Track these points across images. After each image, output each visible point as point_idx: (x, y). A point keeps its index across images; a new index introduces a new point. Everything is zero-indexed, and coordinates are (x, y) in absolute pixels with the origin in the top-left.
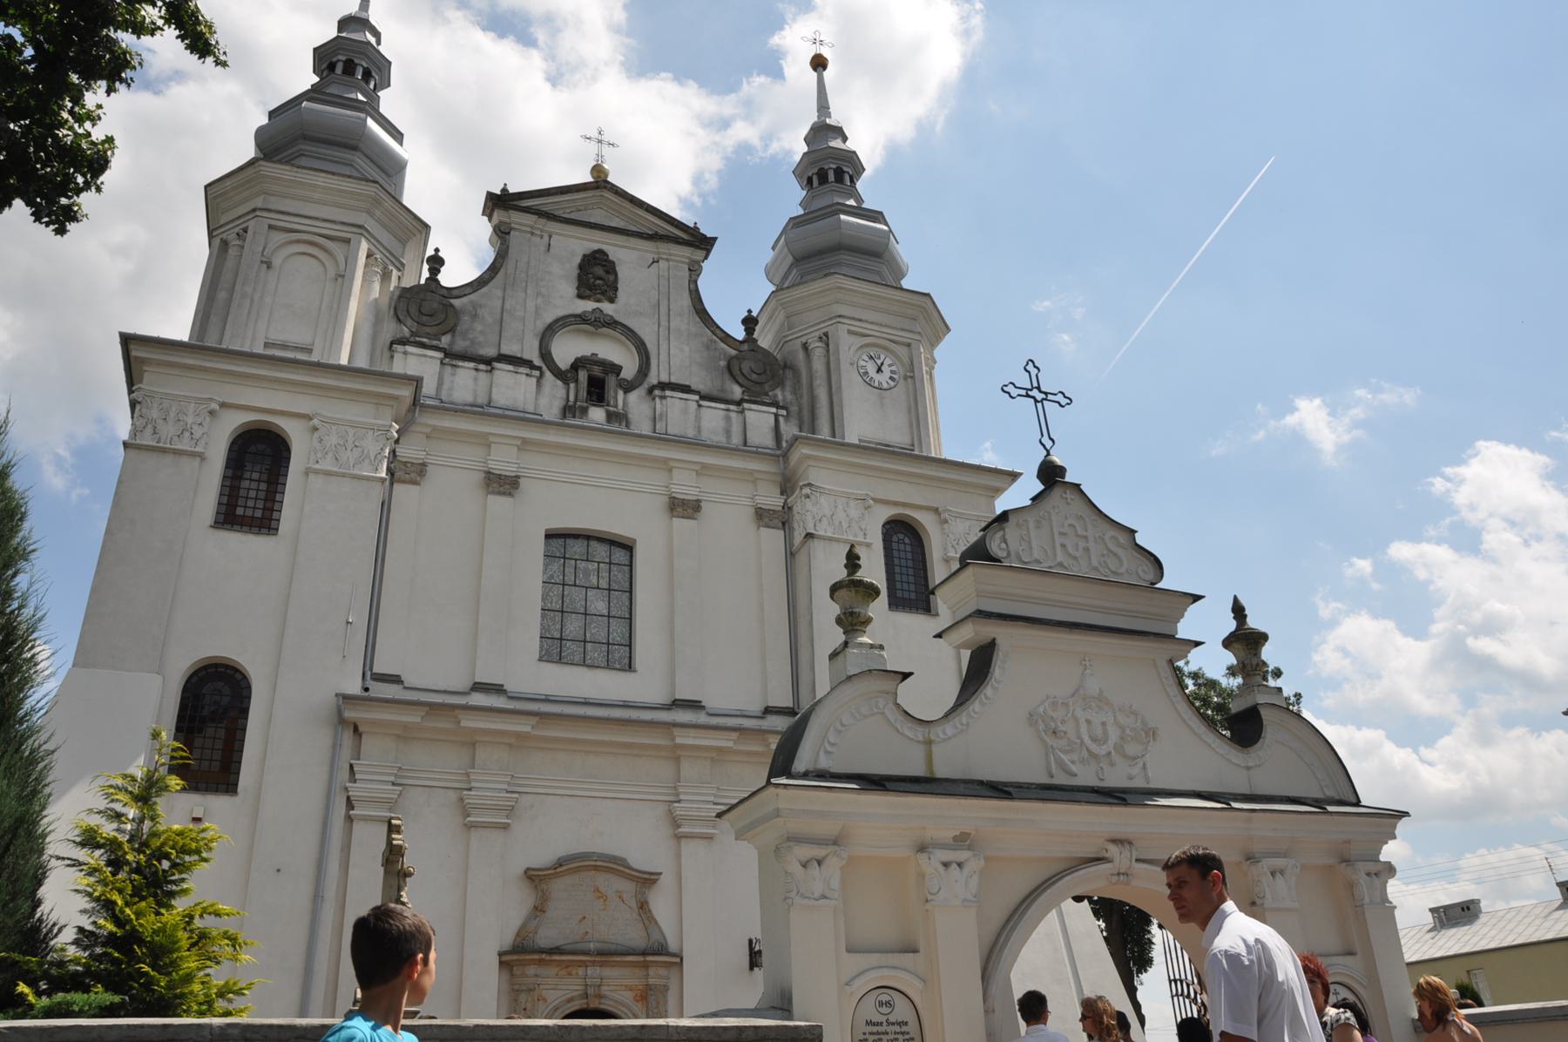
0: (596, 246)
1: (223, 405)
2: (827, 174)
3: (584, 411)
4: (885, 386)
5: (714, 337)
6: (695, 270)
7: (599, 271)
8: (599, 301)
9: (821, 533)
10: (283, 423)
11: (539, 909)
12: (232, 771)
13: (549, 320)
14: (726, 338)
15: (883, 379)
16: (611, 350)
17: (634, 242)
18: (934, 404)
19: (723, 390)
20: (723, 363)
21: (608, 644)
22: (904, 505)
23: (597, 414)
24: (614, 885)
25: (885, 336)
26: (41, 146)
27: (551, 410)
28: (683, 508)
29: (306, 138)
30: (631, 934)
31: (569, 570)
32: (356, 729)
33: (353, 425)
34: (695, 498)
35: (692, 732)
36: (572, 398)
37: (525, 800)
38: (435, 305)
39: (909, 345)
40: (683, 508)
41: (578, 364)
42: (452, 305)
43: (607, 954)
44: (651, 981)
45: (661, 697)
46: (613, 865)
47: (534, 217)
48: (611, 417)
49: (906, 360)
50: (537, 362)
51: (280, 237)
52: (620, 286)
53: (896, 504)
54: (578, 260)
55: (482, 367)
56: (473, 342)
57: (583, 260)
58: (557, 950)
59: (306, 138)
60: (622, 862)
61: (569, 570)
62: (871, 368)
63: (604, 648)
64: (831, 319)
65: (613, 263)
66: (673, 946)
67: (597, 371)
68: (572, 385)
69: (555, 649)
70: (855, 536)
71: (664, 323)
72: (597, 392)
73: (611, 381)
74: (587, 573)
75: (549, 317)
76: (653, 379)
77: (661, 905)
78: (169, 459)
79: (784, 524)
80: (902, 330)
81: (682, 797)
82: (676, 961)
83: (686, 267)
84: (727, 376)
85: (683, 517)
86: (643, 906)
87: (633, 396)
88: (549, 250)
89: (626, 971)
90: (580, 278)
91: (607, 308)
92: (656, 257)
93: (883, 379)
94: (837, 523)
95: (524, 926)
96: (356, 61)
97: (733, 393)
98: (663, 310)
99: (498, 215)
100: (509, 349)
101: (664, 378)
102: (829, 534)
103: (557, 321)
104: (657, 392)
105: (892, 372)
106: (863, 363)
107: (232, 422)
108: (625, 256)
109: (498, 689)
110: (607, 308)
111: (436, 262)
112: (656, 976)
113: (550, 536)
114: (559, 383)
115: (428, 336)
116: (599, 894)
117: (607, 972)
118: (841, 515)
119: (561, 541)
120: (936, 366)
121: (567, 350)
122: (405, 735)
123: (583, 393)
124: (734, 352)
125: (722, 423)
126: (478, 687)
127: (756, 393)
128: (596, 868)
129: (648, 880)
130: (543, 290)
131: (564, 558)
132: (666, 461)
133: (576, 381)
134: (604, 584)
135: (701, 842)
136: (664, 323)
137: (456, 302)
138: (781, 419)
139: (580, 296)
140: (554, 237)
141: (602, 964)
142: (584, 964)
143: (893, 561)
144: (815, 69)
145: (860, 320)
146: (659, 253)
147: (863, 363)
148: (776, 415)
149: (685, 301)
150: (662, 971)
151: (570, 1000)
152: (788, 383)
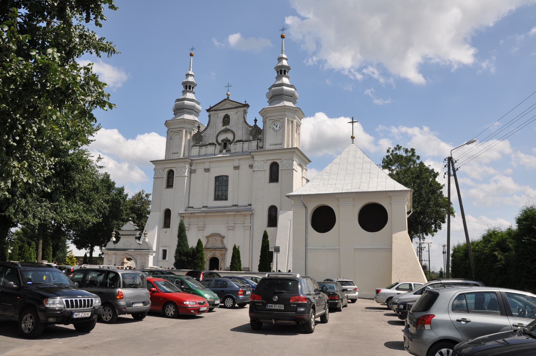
0: (226, 113)
1: (165, 168)
3: (222, 151)
6: (245, 112)
7: (226, 119)
10: (277, 161)
12: (451, 156)
13: (218, 133)
14: (250, 126)
15: (277, 129)
16: (230, 136)
17: (233, 110)
19: (249, 139)
20: (249, 132)
23: (224, 151)
24: (218, 238)
26: (73, 194)
30: (220, 245)
33: (181, 167)
37: (206, 225)
38: (198, 137)
39: (283, 118)
40: (236, 168)
41: (222, 141)
42: (201, 136)
43: (215, 249)
46: (219, 235)
47: (214, 112)
48: (227, 151)
50: (216, 143)
51: (172, 133)
52: (230, 122)
53: (272, 160)
56: (205, 142)
60: (220, 235)
65: (229, 116)
66: (226, 248)
67: (225, 142)
69: (217, 198)
72: (225, 146)
73: (228, 143)
75: (217, 133)
76: (235, 140)
77: (225, 241)
78: (159, 179)
80: (281, 115)
86: (222, 242)
89: (219, 251)
90: (223, 122)
96: (282, 70)
100: (211, 142)
105: (280, 126)
107: (167, 170)
108: (231, 113)
110: (228, 127)
112: (223, 252)
113: (216, 178)
114: (219, 146)
115: (198, 143)
122: (190, 217)
124: (251, 129)
126: (204, 207)
132: (204, 162)
135: (232, 230)
139: (223, 126)
141: (215, 250)
142: (212, 250)
148: (258, 142)
152: (262, 134)
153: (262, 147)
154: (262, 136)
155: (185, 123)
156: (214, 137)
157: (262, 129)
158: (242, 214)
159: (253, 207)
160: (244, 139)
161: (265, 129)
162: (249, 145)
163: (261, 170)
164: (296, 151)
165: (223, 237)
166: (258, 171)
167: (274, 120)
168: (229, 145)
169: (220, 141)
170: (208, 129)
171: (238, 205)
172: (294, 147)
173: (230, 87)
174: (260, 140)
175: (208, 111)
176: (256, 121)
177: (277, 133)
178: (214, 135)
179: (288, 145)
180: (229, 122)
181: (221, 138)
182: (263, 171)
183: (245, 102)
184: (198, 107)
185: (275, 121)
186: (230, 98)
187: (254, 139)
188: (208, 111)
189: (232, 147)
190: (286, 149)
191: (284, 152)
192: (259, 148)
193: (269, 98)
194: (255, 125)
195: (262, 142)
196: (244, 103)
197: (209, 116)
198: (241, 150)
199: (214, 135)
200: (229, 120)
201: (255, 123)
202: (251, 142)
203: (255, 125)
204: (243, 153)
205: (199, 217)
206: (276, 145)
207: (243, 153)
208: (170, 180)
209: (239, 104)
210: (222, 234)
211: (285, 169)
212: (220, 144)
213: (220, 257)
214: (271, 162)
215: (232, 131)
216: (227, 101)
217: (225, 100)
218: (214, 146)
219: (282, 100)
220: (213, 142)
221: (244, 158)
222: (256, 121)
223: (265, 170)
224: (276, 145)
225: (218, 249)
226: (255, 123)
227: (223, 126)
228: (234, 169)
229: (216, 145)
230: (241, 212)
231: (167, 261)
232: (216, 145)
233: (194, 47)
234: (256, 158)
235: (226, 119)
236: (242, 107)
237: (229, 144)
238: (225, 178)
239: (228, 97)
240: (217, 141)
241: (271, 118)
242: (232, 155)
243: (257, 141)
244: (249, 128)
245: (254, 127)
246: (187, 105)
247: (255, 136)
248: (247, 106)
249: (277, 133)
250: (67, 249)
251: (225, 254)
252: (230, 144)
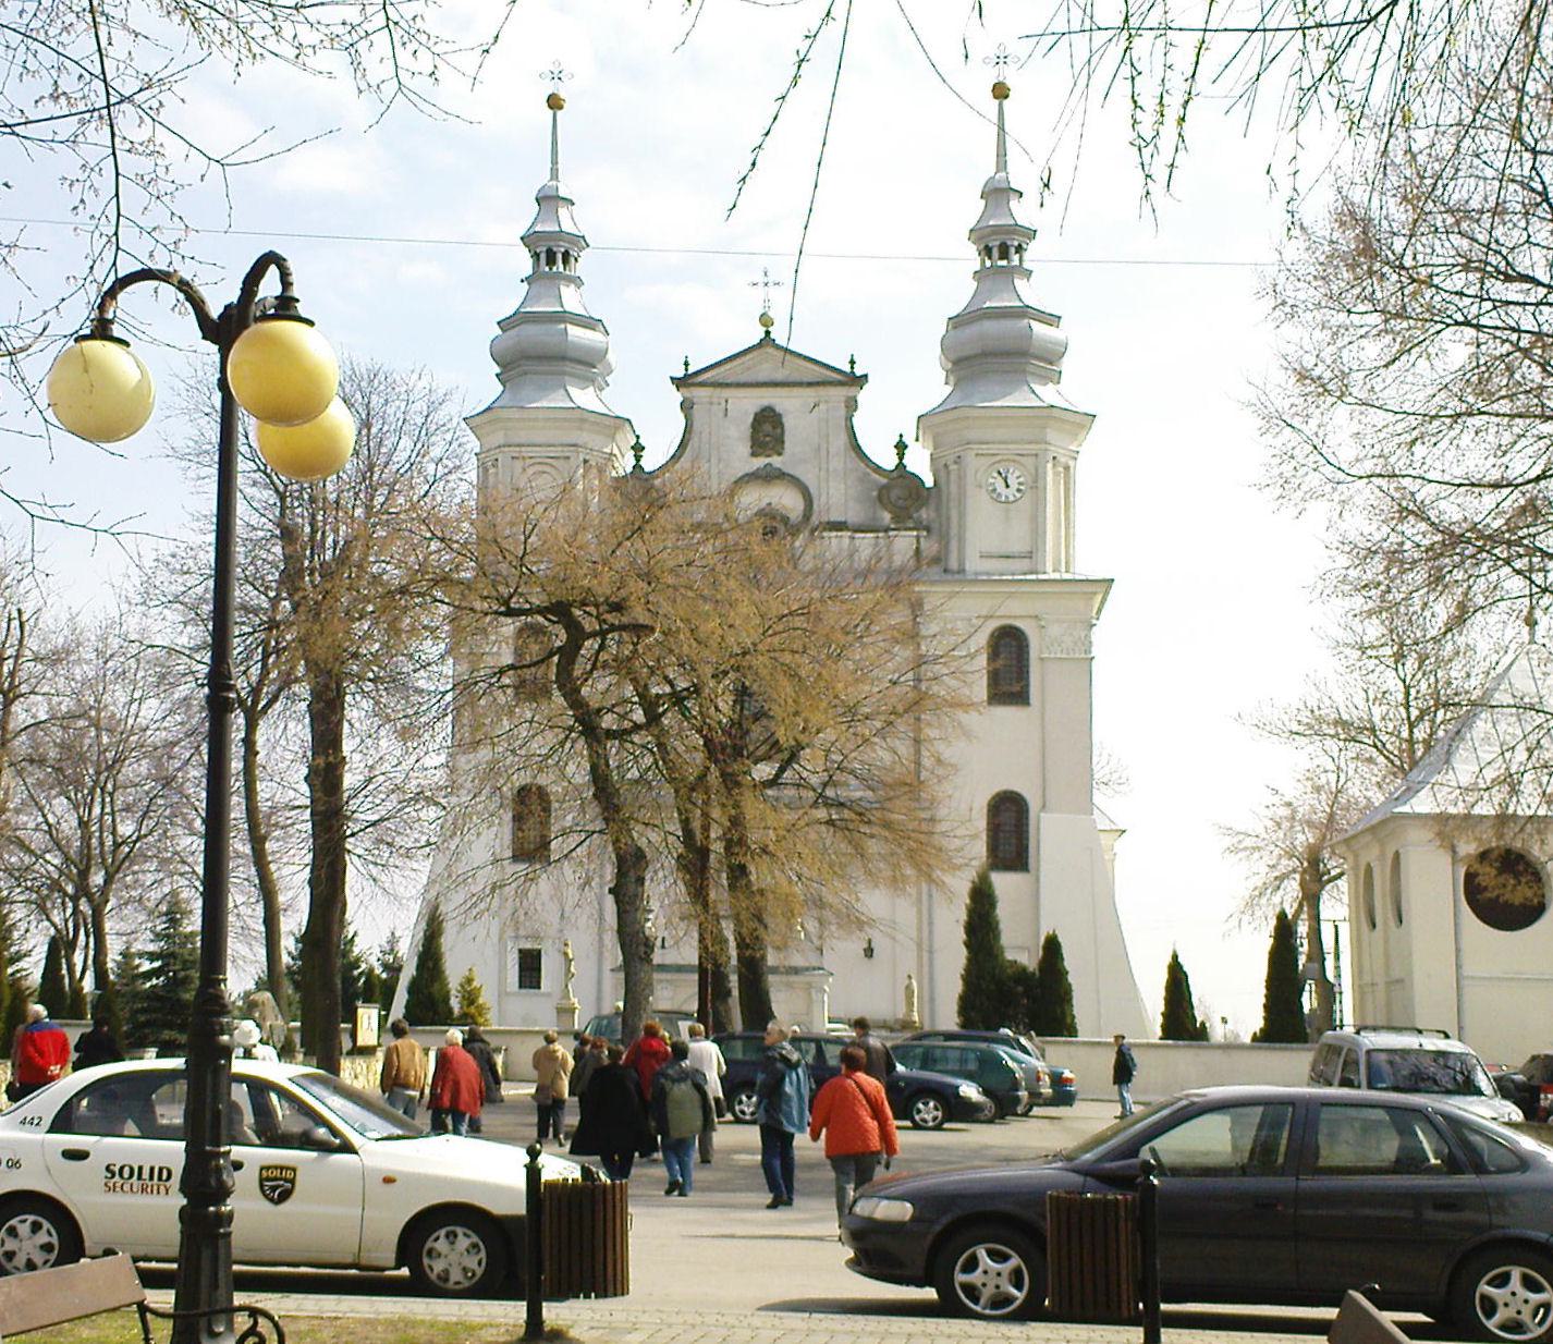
0: (765, 402)
6: (852, 405)
7: (767, 427)
8: (769, 456)
10: (1018, 623)
14: (878, 469)
15: (1011, 493)
16: (787, 501)
17: (796, 391)
18: (1067, 490)
19: (874, 519)
20: (875, 493)
29: (529, 358)
47: (711, 389)
57: (755, 419)
59: (529, 358)
71: (824, 466)
88: (726, 415)
91: (776, 461)
93: (1011, 493)
96: (1009, 243)
98: (823, 453)
99: (688, 392)
105: (1020, 484)
106: (991, 480)
108: (787, 403)
110: (776, 461)
111: (638, 449)
121: (753, 499)
127: (903, 518)
136: (824, 466)
137: (657, 482)
139: (754, 454)
143: (1482, 818)
144: (550, 107)
147: (991, 480)
148: (918, 538)
154: (933, 515)
155: (581, 429)
161: (954, 488)
164: (627, 425)
174: (928, 529)
176: (901, 447)
177: (1007, 510)
183: (852, 362)
185: (999, 462)
188: (679, 383)
191: (1055, 593)
193: (953, 357)
194: (901, 466)
197: (686, 407)
203: (901, 466)
206: (1008, 557)
208: (585, 691)
209: (829, 373)
214: (993, 625)
215: (792, 476)
222: (901, 447)
224: (1008, 557)
227: (754, 454)
231: (543, 995)
235: (767, 427)
236: (841, 384)
239: (768, 333)
243: (915, 533)
246: (579, 347)
249: (1007, 510)
250: (184, 1067)
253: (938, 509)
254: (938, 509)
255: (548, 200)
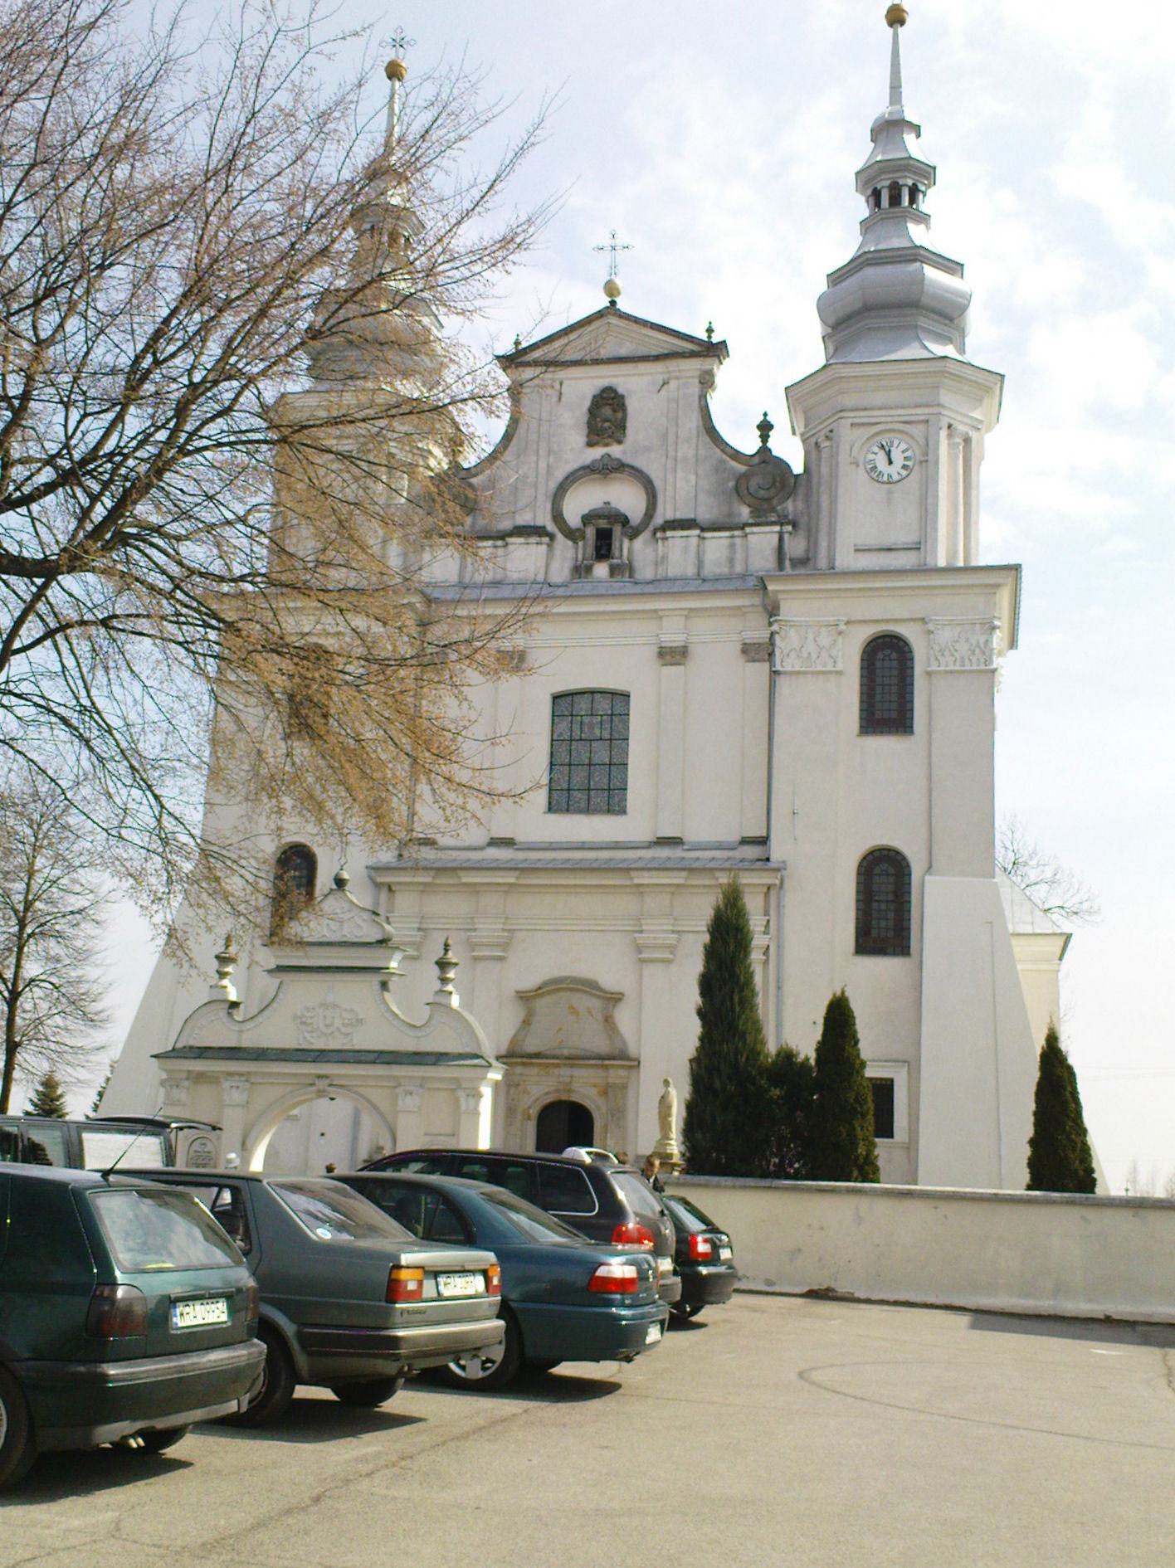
0: (605, 383)
2: (900, 190)
3: (589, 569)
4: (896, 477)
5: (724, 456)
6: (707, 382)
7: (607, 411)
8: (607, 445)
9: (788, 668)
11: (526, 1023)
14: (736, 455)
15: (895, 471)
16: (626, 498)
17: (643, 367)
19: (730, 515)
20: (731, 484)
21: (609, 789)
22: (887, 621)
23: (601, 570)
25: (896, 419)
27: (560, 570)
28: (672, 655)
30: (597, 1042)
31: (576, 727)
32: (390, 889)
34: (682, 644)
35: (646, 874)
36: (580, 557)
37: (519, 935)
40: (672, 655)
41: (587, 519)
43: (575, 1059)
44: (611, 1080)
45: (648, 836)
46: (589, 987)
48: (613, 570)
49: (922, 441)
50: (551, 527)
52: (628, 424)
54: (588, 403)
55: (499, 543)
58: (537, 1055)
61: (576, 727)
62: (881, 460)
63: (606, 794)
64: (834, 414)
65: (623, 397)
66: (633, 1052)
67: (603, 523)
68: (581, 544)
69: (561, 800)
70: (825, 665)
72: (603, 547)
73: (617, 530)
74: (591, 726)
75: (560, 475)
76: (658, 520)
77: (624, 1018)
79: (770, 655)
81: (644, 927)
82: (633, 1064)
83: (696, 381)
84: (735, 497)
85: (671, 665)
86: (608, 1020)
87: (639, 543)
91: (616, 451)
92: (666, 376)
93: (895, 471)
94: (805, 655)
95: (515, 1035)
96: (901, 182)
97: (740, 515)
100: (524, 519)
101: (670, 516)
102: (797, 668)
103: (567, 478)
104: (659, 535)
105: (906, 459)
108: (633, 383)
109: (508, 843)
110: (616, 451)
112: (616, 1075)
113: (556, 698)
114: (570, 543)
116: (574, 1011)
117: (576, 1072)
118: (810, 646)
119: (569, 699)
120: (998, 427)
123: (590, 550)
125: (726, 553)
128: (571, 990)
129: (615, 999)
130: (555, 447)
131: (572, 715)
132: (656, 611)
133: (584, 538)
134: (606, 735)
138: (786, 537)
139: (590, 444)
140: (566, 383)
141: (572, 1066)
142: (557, 1066)
145: (865, 409)
146: (669, 372)
147: (871, 457)
149: (693, 421)
150: (622, 1072)
151: (547, 1093)
152: (800, 497)
153: (803, 562)
154: (800, 505)
156: (541, 498)
157: (798, 468)
158: (465, 884)
159: (777, 852)
160: (704, 514)
161: (825, 470)
162: (732, 546)
163: (819, 668)
165: (614, 999)
166: (805, 673)
167: (875, 429)
168: (626, 543)
169: (573, 516)
170: (508, 456)
171: (685, 840)
172: (973, 563)
173: (620, 255)
174: (794, 525)
175: (509, 362)
176: (765, 428)
177: (889, 493)
178: (542, 489)
179: (953, 554)
180: (622, 427)
181: (580, 503)
182: (830, 673)
184: (942, 288)
186: (623, 305)
187: (761, 517)
189: (640, 551)
190: (960, 569)
192: (787, 563)
193: (831, 321)
194: (764, 450)
195: (802, 533)
196: (704, 336)
198: (691, 571)
199: (542, 489)
200: (624, 419)
201: (765, 438)
202: (748, 530)
203: (764, 450)
204: (703, 583)
205: (478, 892)
206: (890, 550)
207: (703, 583)
210: (609, 980)
211: (951, 668)
212: (572, 535)
213: (601, 1101)
214: (868, 632)
216: (614, 320)
217: (600, 315)
218: (546, 540)
219: (912, 332)
220: (539, 523)
221: (717, 609)
222: (765, 428)
223: (839, 673)
224: (890, 550)
225: (588, 1058)
226: (765, 438)
228: (741, 660)
229: (552, 537)
230: (461, 873)
232: (552, 537)
233: (409, 34)
234: (790, 609)
236: (692, 355)
237: (624, 534)
238: (603, 705)
240: (558, 517)
241: (863, 416)
242: (638, 589)
243: (777, 528)
244: (733, 464)
245: (756, 460)
247: (766, 506)
248: (714, 350)
251: (624, 1087)
252: (632, 538)
253: (807, 500)
254: (807, 500)
255: (890, 128)
